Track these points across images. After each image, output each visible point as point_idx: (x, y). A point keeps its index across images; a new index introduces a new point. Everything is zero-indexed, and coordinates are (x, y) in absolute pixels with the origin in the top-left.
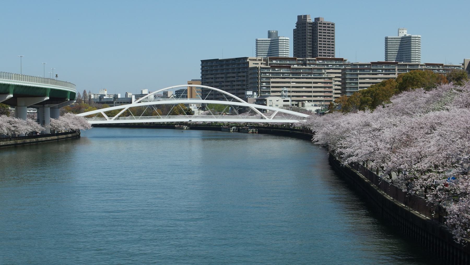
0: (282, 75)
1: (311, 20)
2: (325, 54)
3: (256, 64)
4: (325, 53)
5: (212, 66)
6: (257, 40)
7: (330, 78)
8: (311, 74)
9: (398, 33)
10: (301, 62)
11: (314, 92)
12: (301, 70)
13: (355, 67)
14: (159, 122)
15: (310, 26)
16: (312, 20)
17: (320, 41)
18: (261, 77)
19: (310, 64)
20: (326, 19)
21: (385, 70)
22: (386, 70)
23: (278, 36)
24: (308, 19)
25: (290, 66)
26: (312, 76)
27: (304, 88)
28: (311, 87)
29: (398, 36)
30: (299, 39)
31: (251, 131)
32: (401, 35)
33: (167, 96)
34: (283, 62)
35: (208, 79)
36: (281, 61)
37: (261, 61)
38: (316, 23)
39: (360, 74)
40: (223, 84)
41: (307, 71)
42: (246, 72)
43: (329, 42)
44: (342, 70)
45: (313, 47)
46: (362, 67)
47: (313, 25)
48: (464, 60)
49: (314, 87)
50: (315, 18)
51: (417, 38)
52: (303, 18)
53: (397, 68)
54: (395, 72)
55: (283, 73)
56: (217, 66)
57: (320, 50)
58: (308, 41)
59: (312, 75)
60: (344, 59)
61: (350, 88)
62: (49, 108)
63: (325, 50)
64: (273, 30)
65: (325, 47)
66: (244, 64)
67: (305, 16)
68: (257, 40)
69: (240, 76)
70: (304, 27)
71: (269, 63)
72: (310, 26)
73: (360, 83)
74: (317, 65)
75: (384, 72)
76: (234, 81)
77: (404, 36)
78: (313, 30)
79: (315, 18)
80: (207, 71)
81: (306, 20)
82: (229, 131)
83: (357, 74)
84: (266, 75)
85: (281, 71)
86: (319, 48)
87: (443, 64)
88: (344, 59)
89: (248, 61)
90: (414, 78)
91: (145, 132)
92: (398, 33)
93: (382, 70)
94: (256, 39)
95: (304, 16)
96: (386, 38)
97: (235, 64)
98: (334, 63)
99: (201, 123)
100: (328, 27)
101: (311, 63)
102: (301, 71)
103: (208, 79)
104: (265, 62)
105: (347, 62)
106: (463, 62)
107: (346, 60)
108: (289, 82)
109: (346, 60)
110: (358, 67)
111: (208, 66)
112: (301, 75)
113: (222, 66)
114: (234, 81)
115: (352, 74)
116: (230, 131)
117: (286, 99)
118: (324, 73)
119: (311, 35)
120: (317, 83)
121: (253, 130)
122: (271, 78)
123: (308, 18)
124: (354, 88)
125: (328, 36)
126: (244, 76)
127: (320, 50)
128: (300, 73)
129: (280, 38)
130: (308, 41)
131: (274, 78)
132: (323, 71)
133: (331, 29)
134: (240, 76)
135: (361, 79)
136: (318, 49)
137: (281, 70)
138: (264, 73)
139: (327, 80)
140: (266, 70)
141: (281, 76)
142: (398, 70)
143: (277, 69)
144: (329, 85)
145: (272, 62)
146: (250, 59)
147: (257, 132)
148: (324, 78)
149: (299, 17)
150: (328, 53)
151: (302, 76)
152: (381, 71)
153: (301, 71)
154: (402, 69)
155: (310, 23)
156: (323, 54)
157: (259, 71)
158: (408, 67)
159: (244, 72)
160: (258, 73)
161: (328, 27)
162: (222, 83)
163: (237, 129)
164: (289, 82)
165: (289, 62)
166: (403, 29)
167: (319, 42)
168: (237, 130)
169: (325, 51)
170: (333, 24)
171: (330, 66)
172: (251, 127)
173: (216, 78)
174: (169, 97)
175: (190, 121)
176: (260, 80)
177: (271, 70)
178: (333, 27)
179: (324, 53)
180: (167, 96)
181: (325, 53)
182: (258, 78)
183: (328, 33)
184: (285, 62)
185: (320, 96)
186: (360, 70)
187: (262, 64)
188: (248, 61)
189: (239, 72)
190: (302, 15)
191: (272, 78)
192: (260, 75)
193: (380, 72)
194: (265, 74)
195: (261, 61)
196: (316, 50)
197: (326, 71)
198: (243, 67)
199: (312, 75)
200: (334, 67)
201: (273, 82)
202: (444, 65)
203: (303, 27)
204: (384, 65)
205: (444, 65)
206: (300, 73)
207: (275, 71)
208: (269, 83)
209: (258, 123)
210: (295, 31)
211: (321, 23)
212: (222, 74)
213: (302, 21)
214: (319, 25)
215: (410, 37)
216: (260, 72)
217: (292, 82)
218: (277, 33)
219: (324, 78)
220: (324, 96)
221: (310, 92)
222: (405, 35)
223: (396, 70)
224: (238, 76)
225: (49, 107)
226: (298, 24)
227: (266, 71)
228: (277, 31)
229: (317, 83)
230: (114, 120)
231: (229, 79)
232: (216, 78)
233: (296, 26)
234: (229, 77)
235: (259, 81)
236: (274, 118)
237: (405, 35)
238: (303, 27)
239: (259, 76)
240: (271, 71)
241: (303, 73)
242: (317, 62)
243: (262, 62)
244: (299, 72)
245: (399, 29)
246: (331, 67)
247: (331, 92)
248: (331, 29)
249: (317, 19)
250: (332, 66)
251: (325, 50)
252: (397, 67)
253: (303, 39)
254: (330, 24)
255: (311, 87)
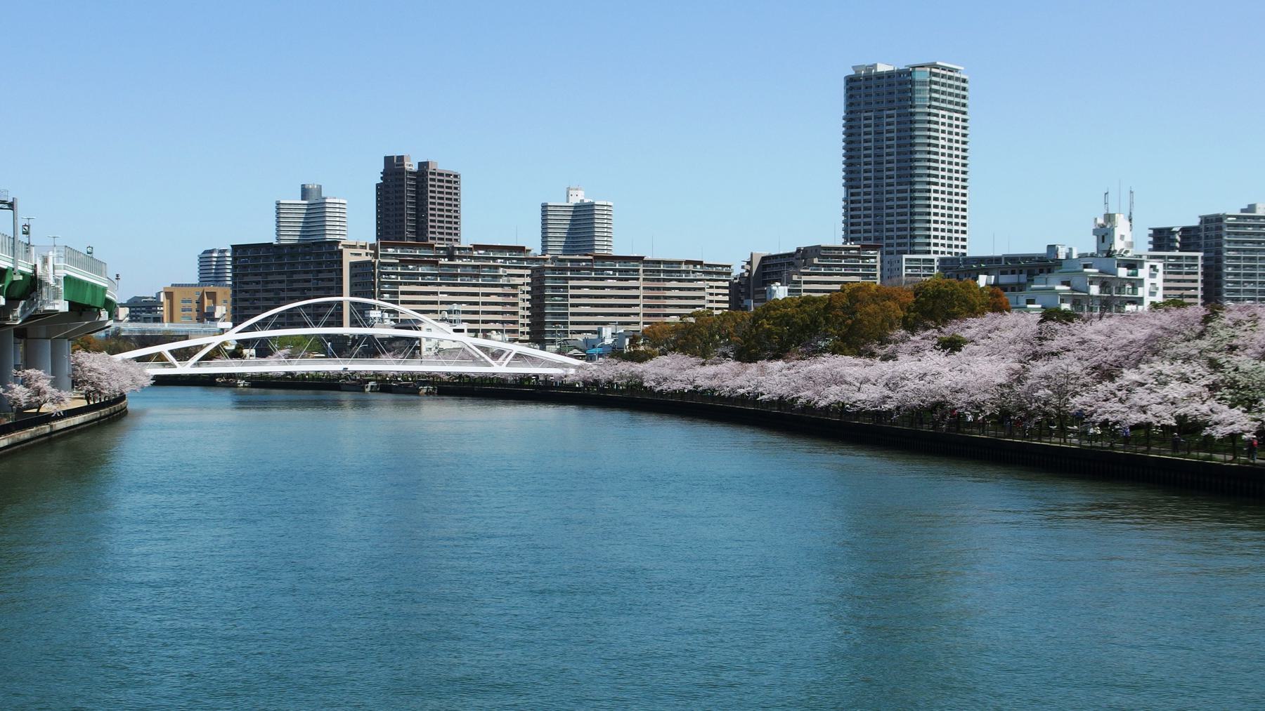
0: (422, 279)
1: (412, 165)
2: (442, 236)
3: (356, 254)
4: (442, 233)
5: (255, 258)
6: (278, 204)
7: (514, 286)
8: (477, 276)
9: (568, 196)
10: (444, 253)
11: (484, 312)
12: (459, 270)
13: (562, 265)
14: (267, 373)
15: (411, 179)
16: (415, 168)
17: (431, 209)
18: (379, 281)
19: (460, 257)
20: (442, 163)
21: (620, 272)
22: (620, 271)
23: (323, 195)
24: (406, 163)
25: (437, 261)
26: (480, 282)
27: (463, 305)
28: (476, 303)
29: (568, 202)
30: (387, 204)
31: (425, 391)
32: (574, 201)
33: (116, 318)
34: (407, 252)
35: (247, 283)
36: (403, 249)
37: (366, 249)
38: (425, 173)
39: (572, 279)
40: (282, 295)
41: (469, 271)
42: (335, 270)
43: (449, 211)
44: (533, 269)
45: (417, 221)
46: (575, 265)
47: (418, 176)
48: (752, 255)
49: (484, 304)
50: (419, 163)
51: (605, 208)
52: (395, 161)
53: (641, 268)
54: (876, 279)
55: (423, 275)
56: (267, 257)
57: (432, 227)
58: (409, 210)
59: (480, 280)
60: (527, 248)
61: (553, 305)
62: (49, 341)
63: (442, 227)
64: (311, 183)
65: (442, 222)
66: (331, 254)
67: (401, 158)
68: (278, 204)
69: (322, 280)
70: (400, 180)
71: (380, 252)
72: (411, 179)
73: (572, 296)
74: (475, 258)
75: (617, 276)
76: (283, 290)
77: (579, 202)
78: (417, 186)
79: (419, 163)
80: (245, 267)
81: (403, 165)
82: (362, 390)
83: (567, 279)
84: (390, 279)
85: (420, 271)
86: (430, 224)
87: (702, 262)
88: (527, 248)
89: (340, 247)
90: (952, 294)
91: (195, 392)
92: (568, 196)
93: (615, 270)
94: (277, 201)
95: (398, 157)
96: (545, 207)
97: (310, 254)
98: (508, 256)
99: (510, 379)
100: (448, 182)
101: (463, 255)
102: (459, 271)
103: (247, 283)
104: (373, 252)
105: (531, 255)
106: (748, 258)
107: (530, 250)
108: (435, 293)
109: (530, 250)
110: (569, 266)
111: (248, 257)
112: (459, 279)
113: (280, 257)
114: (283, 290)
115: (555, 278)
116: (364, 391)
117: (459, 327)
118: (501, 276)
119: (413, 197)
120: (488, 295)
121: (428, 388)
122: (401, 284)
123: (408, 161)
124: (559, 305)
125: (447, 199)
126: (331, 280)
127: (432, 227)
128: (456, 276)
129: (327, 201)
130: (409, 210)
131: (405, 284)
132: (501, 271)
133: (454, 185)
134: (322, 280)
135: (573, 287)
136: (427, 226)
137: (420, 268)
138: (385, 274)
139: (508, 290)
140: (390, 268)
141: (420, 280)
142: (644, 271)
143: (411, 267)
144: (511, 300)
145: (387, 251)
146: (343, 245)
147: (436, 392)
148: (502, 286)
149: (388, 160)
150: (447, 234)
151: (461, 280)
152: (611, 272)
153: (457, 271)
154: (650, 271)
155: (411, 173)
156: (438, 236)
157: (377, 270)
158: (662, 266)
159: (330, 271)
160: (373, 274)
161: (448, 182)
162: (281, 293)
163: (378, 386)
164: (435, 293)
165: (419, 252)
166: (577, 189)
167: (430, 212)
168: (378, 389)
169: (442, 231)
170: (456, 176)
171: (499, 261)
172: (424, 383)
173: (267, 282)
174: (121, 321)
175: (345, 369)
176: (379, 287)
177: (399, 268)
178: (457, 182)
179: (440, 233)
180: (116, 318)
181: (442, 233)
182: (373, 284)
183: (447, 193)
184: (411, 252)
185: (495, 322)
186: (572, 270)
187: (367, 254)
188: (340, 247)
189: (320, 272)
190: (393, 157)
191: (401, 285)
192: (378, 278)
193: (609, 274)
194: (388, 275)
195: (366, 249)
196: (425, 227)
197: (505, 272)
198: (329, 261)
199: (480, 280)
200: (508, 264)
201: (403, 293)
202: (704, 263)
203: (396, 179)
204: (617, 261)
205: (704, 263)
206: (456, 276)
207: (409, 269)
208: (396, 293)
209: (439, 374)
210: (380, 189)
211: (434, 174)
212: (280, 273)
213: (393, 167)
214: (430, 176)
215: (593, 205)
216: (379, 272)
217: (441, 293)
218: (320, 188)
219: (502, 286)
220: (502, 322)
221: (476, 313)
222: (581, 200)
223: (641, 271)
224: (318, 280)
225: (48, 339)
226: (386, 174)
227: (390, 269)
228: (321, 186)
229: (488, 295)
230: (191, 367)
231: (295, 286)
232: (267, 282)
233: (382, 178)
234: (296, 281)
235: (377, 289)
236: (508, 365)
237: (582, 201)
238: (396, 179)
239: (377, 280)
240: (399, 271)
241: (461, 275)
242: (475, 253)
243: (368, 250)
244: (455, 272)
245: (569, 189)
246: (501, 262)
247: (515, 313)
248: (454, 185)
249: (423, 165)
250: (503, 260)
251: (442, 227)
252: (642, 265)
253: (396, 203)
254: (451, 175)
255: (476, 303)
